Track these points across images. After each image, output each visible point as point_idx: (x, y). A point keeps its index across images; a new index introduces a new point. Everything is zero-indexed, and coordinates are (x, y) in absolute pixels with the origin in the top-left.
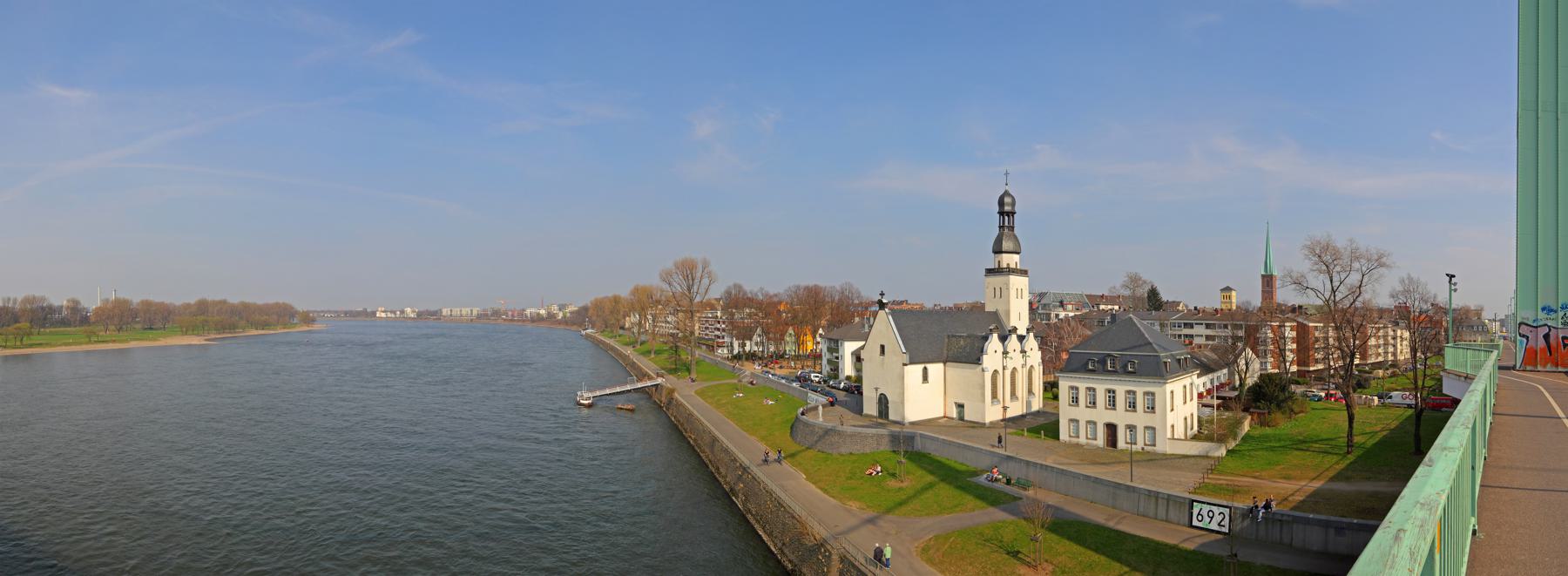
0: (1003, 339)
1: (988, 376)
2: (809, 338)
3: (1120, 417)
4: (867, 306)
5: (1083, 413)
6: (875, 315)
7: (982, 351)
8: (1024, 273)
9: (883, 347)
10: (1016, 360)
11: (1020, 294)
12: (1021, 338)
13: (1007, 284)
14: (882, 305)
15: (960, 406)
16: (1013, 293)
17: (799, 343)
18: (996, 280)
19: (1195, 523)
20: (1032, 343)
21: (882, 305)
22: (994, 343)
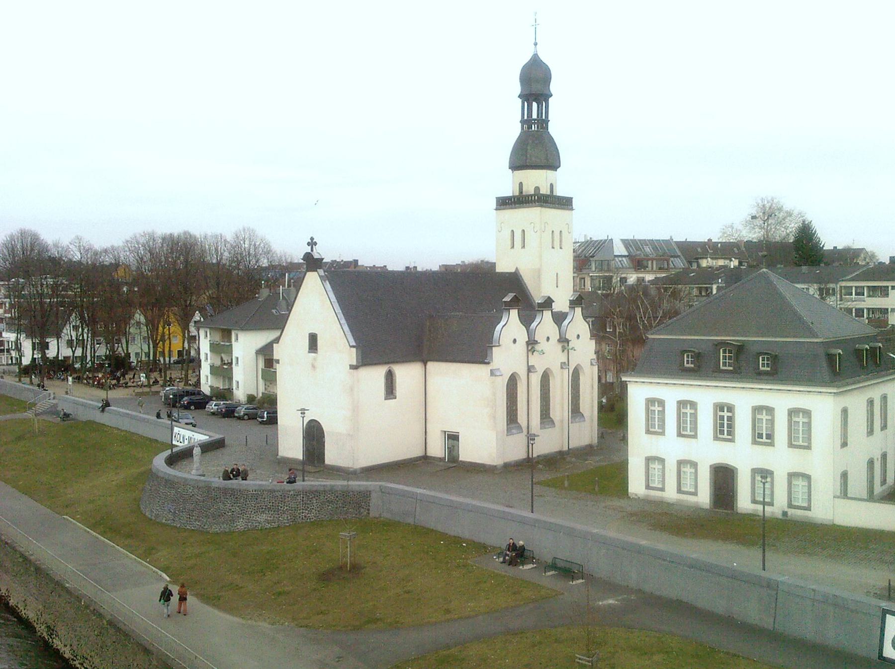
0: (527, 321)
1: (502, 383)
2: (175, 328)
3: (742, 455)
4: (291, 267)
6: (297, 284)
9: (313, 342)
10: (550, 356)
12: (559, 318)
17: (155, 339)
20: (579, 326)
22: (510, 327)
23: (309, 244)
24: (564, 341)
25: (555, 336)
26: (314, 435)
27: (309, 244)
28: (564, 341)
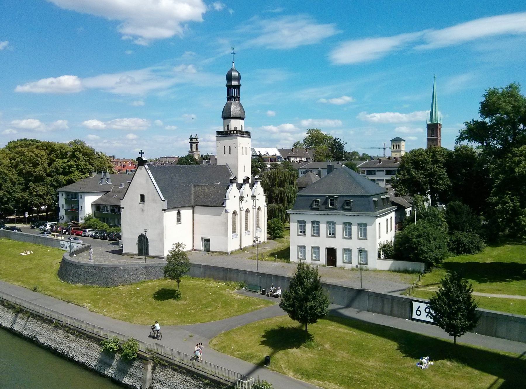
1: (230, 215)
3: (339, 243)
5: (308, 241)
7: (224, 199)
8: (247, 134)
9: (142, 197)
10: (248, 203)
11: (245, 152)
12: (240, 187)
13: (235, 144)
14: (141, 162)
15: (206, 241)
16: (240, 150)
18: (227, 142)
19: (415, 316)
21: (141, 162)
22: (233, 191)
23: (140, 153)
24: (254, 197)
25: (238, 196)
26: (143, 242)
27: (140, 153)
28: (254, 197)
